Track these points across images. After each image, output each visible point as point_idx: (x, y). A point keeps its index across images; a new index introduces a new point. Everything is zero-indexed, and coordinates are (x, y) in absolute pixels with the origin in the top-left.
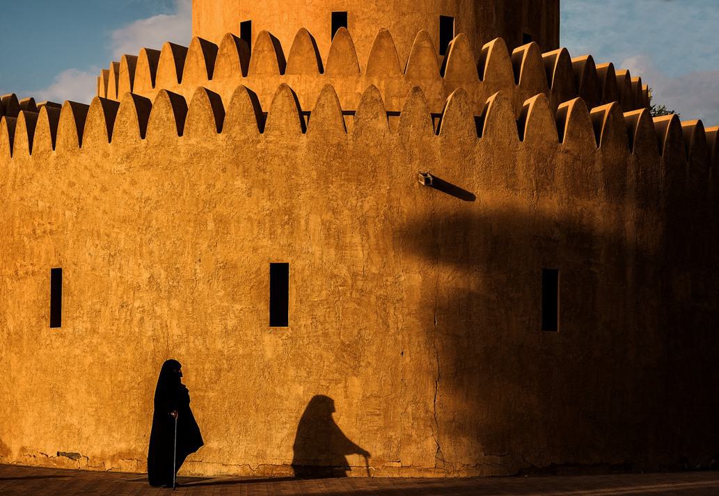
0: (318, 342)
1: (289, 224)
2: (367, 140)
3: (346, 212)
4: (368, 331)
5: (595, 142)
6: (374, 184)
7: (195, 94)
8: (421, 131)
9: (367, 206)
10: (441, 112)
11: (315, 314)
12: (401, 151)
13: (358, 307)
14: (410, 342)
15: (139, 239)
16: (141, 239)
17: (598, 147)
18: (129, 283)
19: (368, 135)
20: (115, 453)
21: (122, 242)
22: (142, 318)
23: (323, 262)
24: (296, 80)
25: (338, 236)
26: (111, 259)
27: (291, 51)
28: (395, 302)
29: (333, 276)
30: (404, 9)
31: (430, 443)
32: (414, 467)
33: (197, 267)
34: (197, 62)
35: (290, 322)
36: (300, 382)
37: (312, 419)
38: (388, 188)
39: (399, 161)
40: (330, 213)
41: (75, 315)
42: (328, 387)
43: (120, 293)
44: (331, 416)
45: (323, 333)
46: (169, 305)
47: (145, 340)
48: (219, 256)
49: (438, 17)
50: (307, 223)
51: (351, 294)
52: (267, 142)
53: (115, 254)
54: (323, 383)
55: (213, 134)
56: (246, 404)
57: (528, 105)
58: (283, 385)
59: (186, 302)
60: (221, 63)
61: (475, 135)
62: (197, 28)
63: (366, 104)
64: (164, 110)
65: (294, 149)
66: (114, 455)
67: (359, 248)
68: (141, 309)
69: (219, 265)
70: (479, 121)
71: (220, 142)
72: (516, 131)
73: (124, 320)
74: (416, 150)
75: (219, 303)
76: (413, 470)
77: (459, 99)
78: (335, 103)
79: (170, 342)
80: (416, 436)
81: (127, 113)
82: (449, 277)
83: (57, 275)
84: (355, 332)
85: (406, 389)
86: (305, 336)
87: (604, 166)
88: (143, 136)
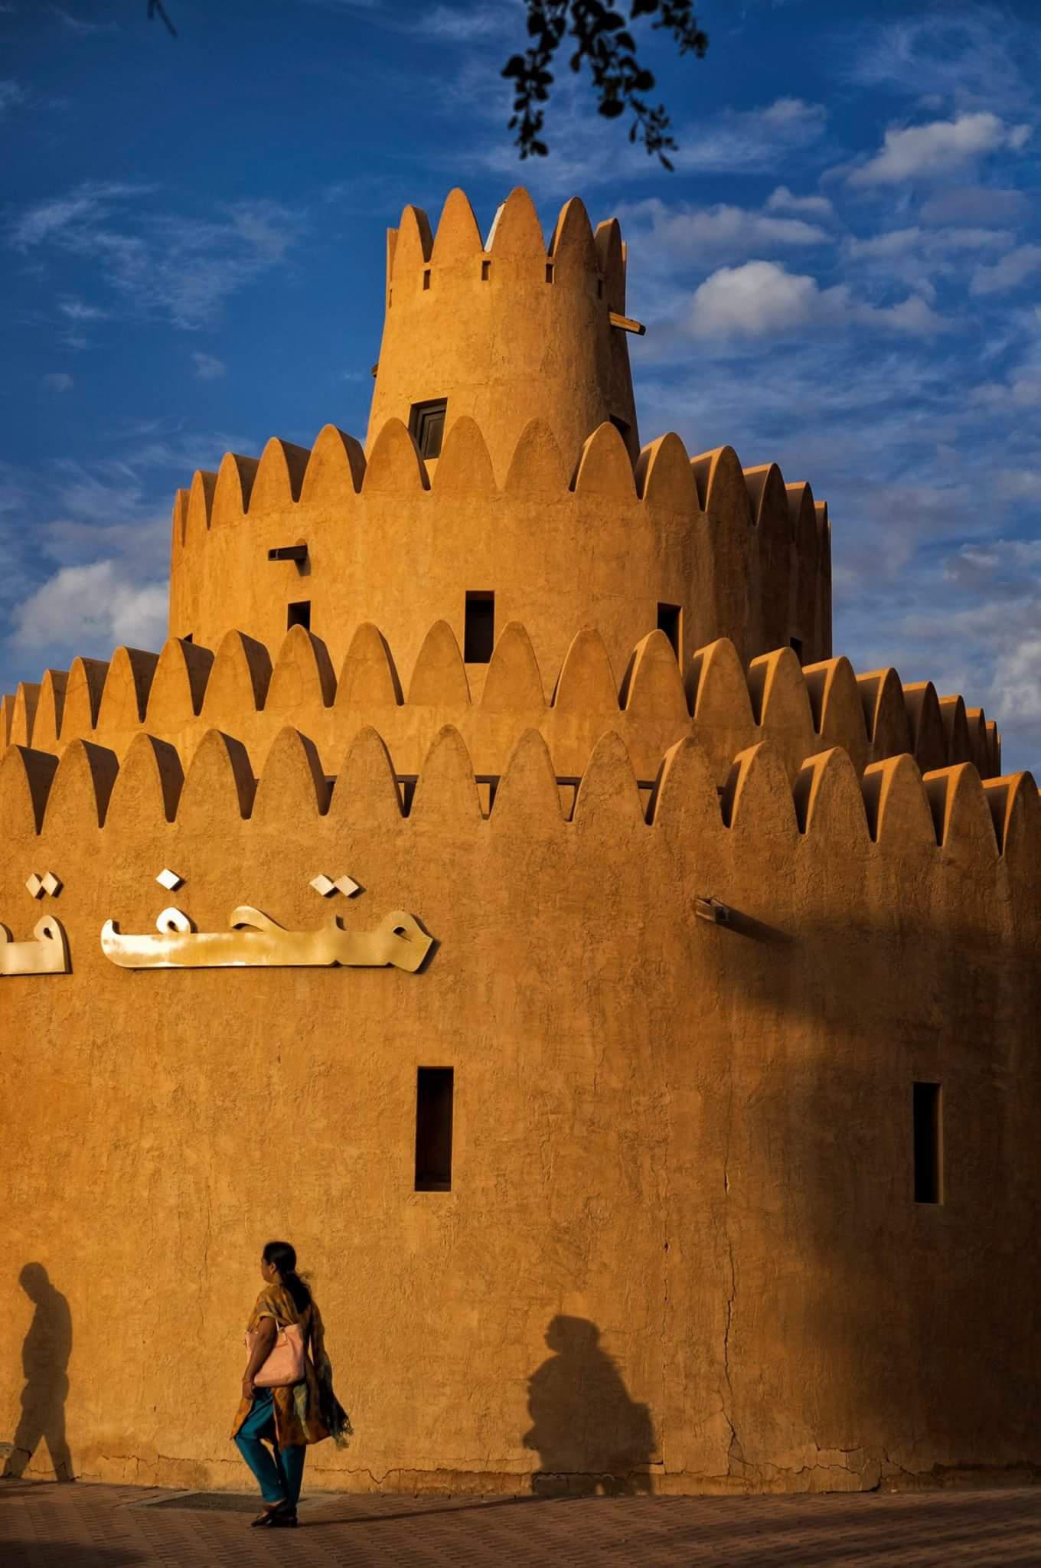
0: (509, 1223)
1: (454, 991)
2: (602, 833)
4: (603, 1202)
5: (996, 845)
6: (614, 918)
7: (277, 740)
8: (701, 818)
9: (601, 960)
10: (653, 779)
11: (503, 1167)
12: (664, 856)
13: (584, 1155)
14: (680, 1225)
15: (156, 1016)
16: (160, 1015)
17: (1001, 853)
18: (132, 1100)
19: (604, 825)
20: (89, 1443)
21: (121, 1020)
22: (157, 1172)
23: (518, 1065)
24: (427, 715)
25: (548, 1015)
26: (96, 1053)
27: (418, 661)
28: (652, 1144)
29: (538, 1094)
31: (719, 1426)
32: (690, 1474)
33: (274, 1071)
34: (235, 676)
35: (455, 1182)
36: (473, 1302)
37: (494, 1376)
38: (641, 925)
39: (659, 875)
40: (534, 972)
41: (13, 1162)
42: (527, 1312)
43: (111, 1121)
45: (518, 1205)
46: (212, 1145)
47: (161, 1215)
48: (317, 1052)
49: (656, 607)
50: (489, 989)
51: (572, 1128)
52: (415, 834)
53: (105, 1043)
54: (517, 1303)
55: (311, 815)
56: (365, 1345)
57: (811, 769)
58: (439, 1309)
59: (248, 1140)
60: (281, 685)
61: (795, 828)
62: (189, 610)
63: (600, 767)
64: (215, 769)
65: (467, 848)
66: (88, 1449)
67: (587, 1040)
68: (157, 1153)
69: (316, 1069)
70: (726, 794)
71: (324, 832)
72: (865, 823)
73: (117, 1175)
74: (691, 855)
75: (314, 1143)
76: (687, 1480)
77: (766, 761)
78: (544, 764)
79: (214, 1219)
80: (692, 1412)
81: (139, 773)
82: (750, 1098)
84: (580, 1203)
85: (673, 1318)
86: (484, 1210)
87: (1012, 890)
88: (170, 816)
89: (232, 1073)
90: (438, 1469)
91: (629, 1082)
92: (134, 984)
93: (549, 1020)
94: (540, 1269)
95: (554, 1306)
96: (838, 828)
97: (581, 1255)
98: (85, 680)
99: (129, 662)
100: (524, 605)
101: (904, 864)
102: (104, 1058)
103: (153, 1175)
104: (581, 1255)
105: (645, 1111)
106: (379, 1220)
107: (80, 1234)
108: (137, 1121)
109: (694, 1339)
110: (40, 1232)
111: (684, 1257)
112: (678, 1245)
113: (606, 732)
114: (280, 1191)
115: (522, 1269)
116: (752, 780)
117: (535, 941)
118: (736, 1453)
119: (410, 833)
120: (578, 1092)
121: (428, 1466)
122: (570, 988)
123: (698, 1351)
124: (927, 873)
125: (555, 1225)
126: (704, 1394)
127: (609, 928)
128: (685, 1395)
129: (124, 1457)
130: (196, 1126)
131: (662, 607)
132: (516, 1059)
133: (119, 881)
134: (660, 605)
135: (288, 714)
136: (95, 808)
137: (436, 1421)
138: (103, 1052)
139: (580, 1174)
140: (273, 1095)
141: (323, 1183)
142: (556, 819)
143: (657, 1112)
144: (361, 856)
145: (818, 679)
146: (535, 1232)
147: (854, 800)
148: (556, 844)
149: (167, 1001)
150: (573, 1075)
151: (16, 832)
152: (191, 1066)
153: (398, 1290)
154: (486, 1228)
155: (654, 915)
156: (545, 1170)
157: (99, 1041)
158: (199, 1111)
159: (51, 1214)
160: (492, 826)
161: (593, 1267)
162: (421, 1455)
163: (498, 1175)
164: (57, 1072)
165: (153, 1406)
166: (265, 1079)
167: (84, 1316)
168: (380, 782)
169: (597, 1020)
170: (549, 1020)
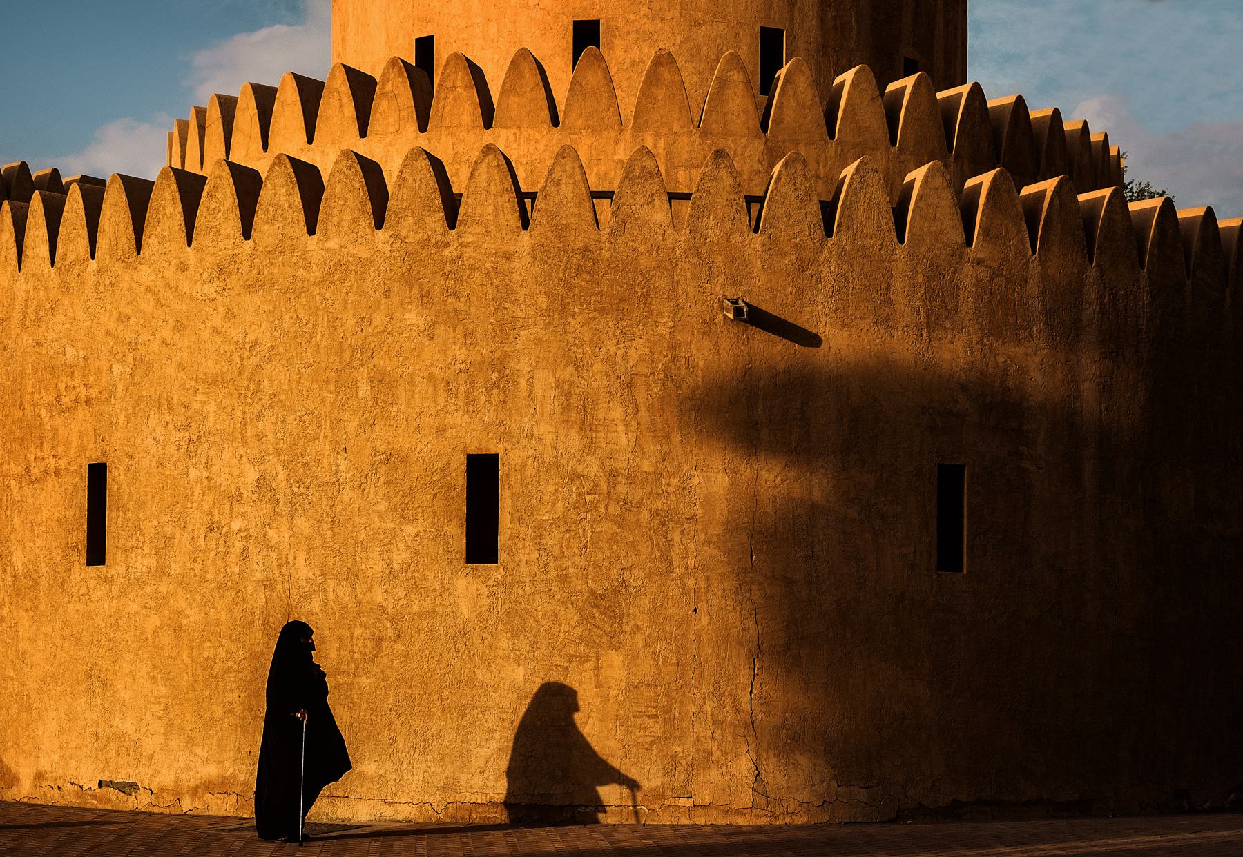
2: (634, 241)
4: (636, 572)
5: (1028, 245)
6: (646, 318)
8: (728, 225)
9: (633, 356)
10: (762, 194)
11: (544, 541)
13: (618, 530)
16: (244, 413)
17: (1034, 253)
20: (198, 782)
21: (211, 419)
22: (246, 550)
23: (558, 452)
24: (512, 138)
26: (192, 448)
29: (576, 477)
32: (716, 807)
33: (341, 461)
35: (502, 557)
38: (671, 324)
40: (570, 368)
41: (129, 544)
42: (567, 668)
43: (206, 507)
46: (291, 526)
47: (250, 588)
48: (378, 443)
49: (758, 30)
50: (531, 385)
51: (607, 507)
52: (461, 245)
53: (199, 439)
55: (368, 231)
57: (912, 182)
59: (321, 521)
60: (381, 109)
61: (820, 232)
63: (632, 179)
64: (283, 191)
65: (508, 256)
66: (197, 787)
67: (621, 428)
68: (245, 534)
69: (378, 458)
70: (828, 209)
72: (893, 227)
73: (213, 553)
74: (719, 259)
75: (377, 523)
78: (579, 178)
80: (718, 753)
85: (701, 673)
86: (528, 580)
88: (247, 234)
89: (306, 463)
90: (490, 802)
91: (660, 466)
92: (220, 386)
93: (585, 411)
94: (578, 631)
95: (592, 663)
96: (865, 231)
97: (615, 618)
98: (220, 115)
99: (253, 97)
100: (629, 33)
101: (932, 265)
102: (199, 452)
103: (243, 553)
104: (615, 618)
105: (674, 492)
106: (434, 589)
107: (184, 605)
108: (228, 506)
109: (721, 691)
110: (152, 604)
111: (711, 619)
112: (705, 610)
113: (638, 147)
114: (349, 565)
115: (563, 631)
116: (779, 188)
117: (571, 340)
118: (760, 789)
119: (456, 244)
120: (612, 476)
121: (481, 799)
122: (605, 382)
123: (724, 701)
124: (955, 273)
125: (592, 593)
126: (730, 738)
127: (641, 327)
128: (713, 739)
129: (226, 793)
130: (276, 510)
131: (764, 31)
132: (555, 447)
133: (206, 295)
134: (762, 29)
135: (388, 140)
136: (184, 229)
137: (487, 762)
138: (198, 447)
139: (615, 547)
140: (341, 481)
141: (386, 558)
142: (591, 228)
143: (686, 492)
144: (413, 266)
145: (953, 101)
146: (573, 598)
147: (881, 205)
148: (590, 251)
149: (249, 400)
150: (608, 460)
151: (120, 253)
152: (271, 457)
153: (453, 649)
154: (529, 595)
155: (683, 314)
156: (583, 544)
157: (194, 438)
158: (278, 496)
159: (161, 588)
160: (531, 236)
161: (627, 628)
162: (474, 791)
163: (539, 550)
164: (161, 464)
165: (248, 750)
166: (334, 468)
167: (190, 674)
168: (429, 197)
169: (629, 411)
170: (585, 411)
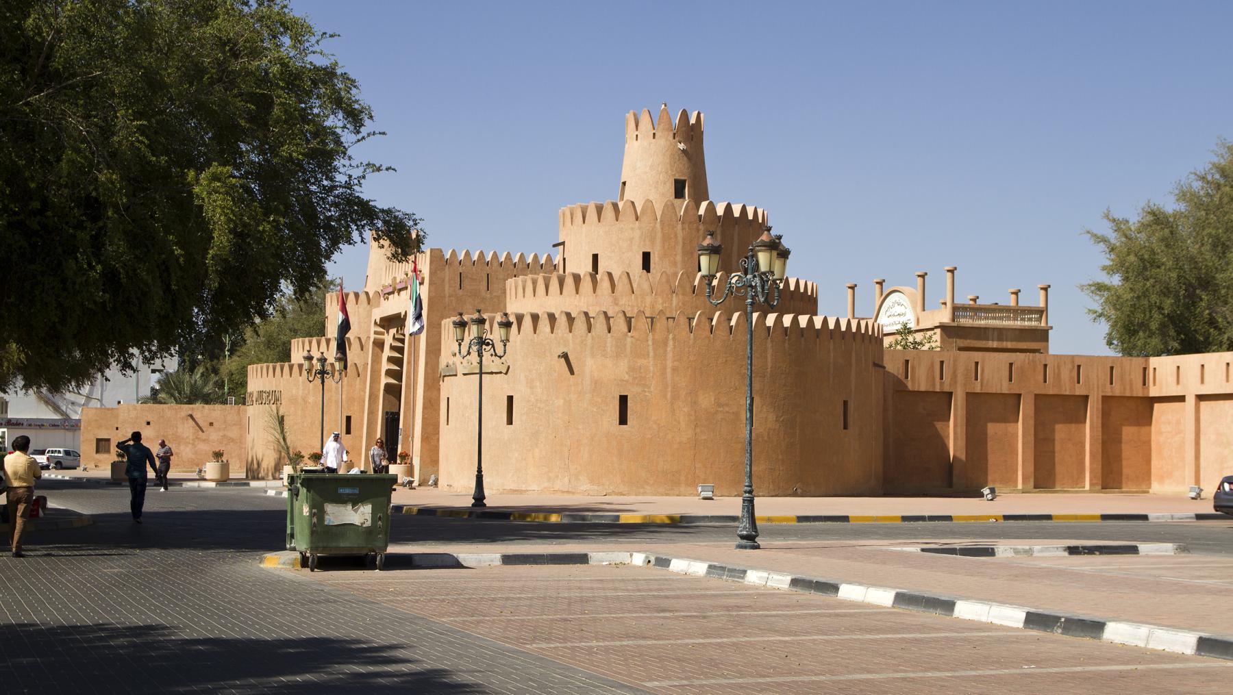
3: (534, 371)
30: (624, 250)
44: (986, 425)
83: (448, 398)
